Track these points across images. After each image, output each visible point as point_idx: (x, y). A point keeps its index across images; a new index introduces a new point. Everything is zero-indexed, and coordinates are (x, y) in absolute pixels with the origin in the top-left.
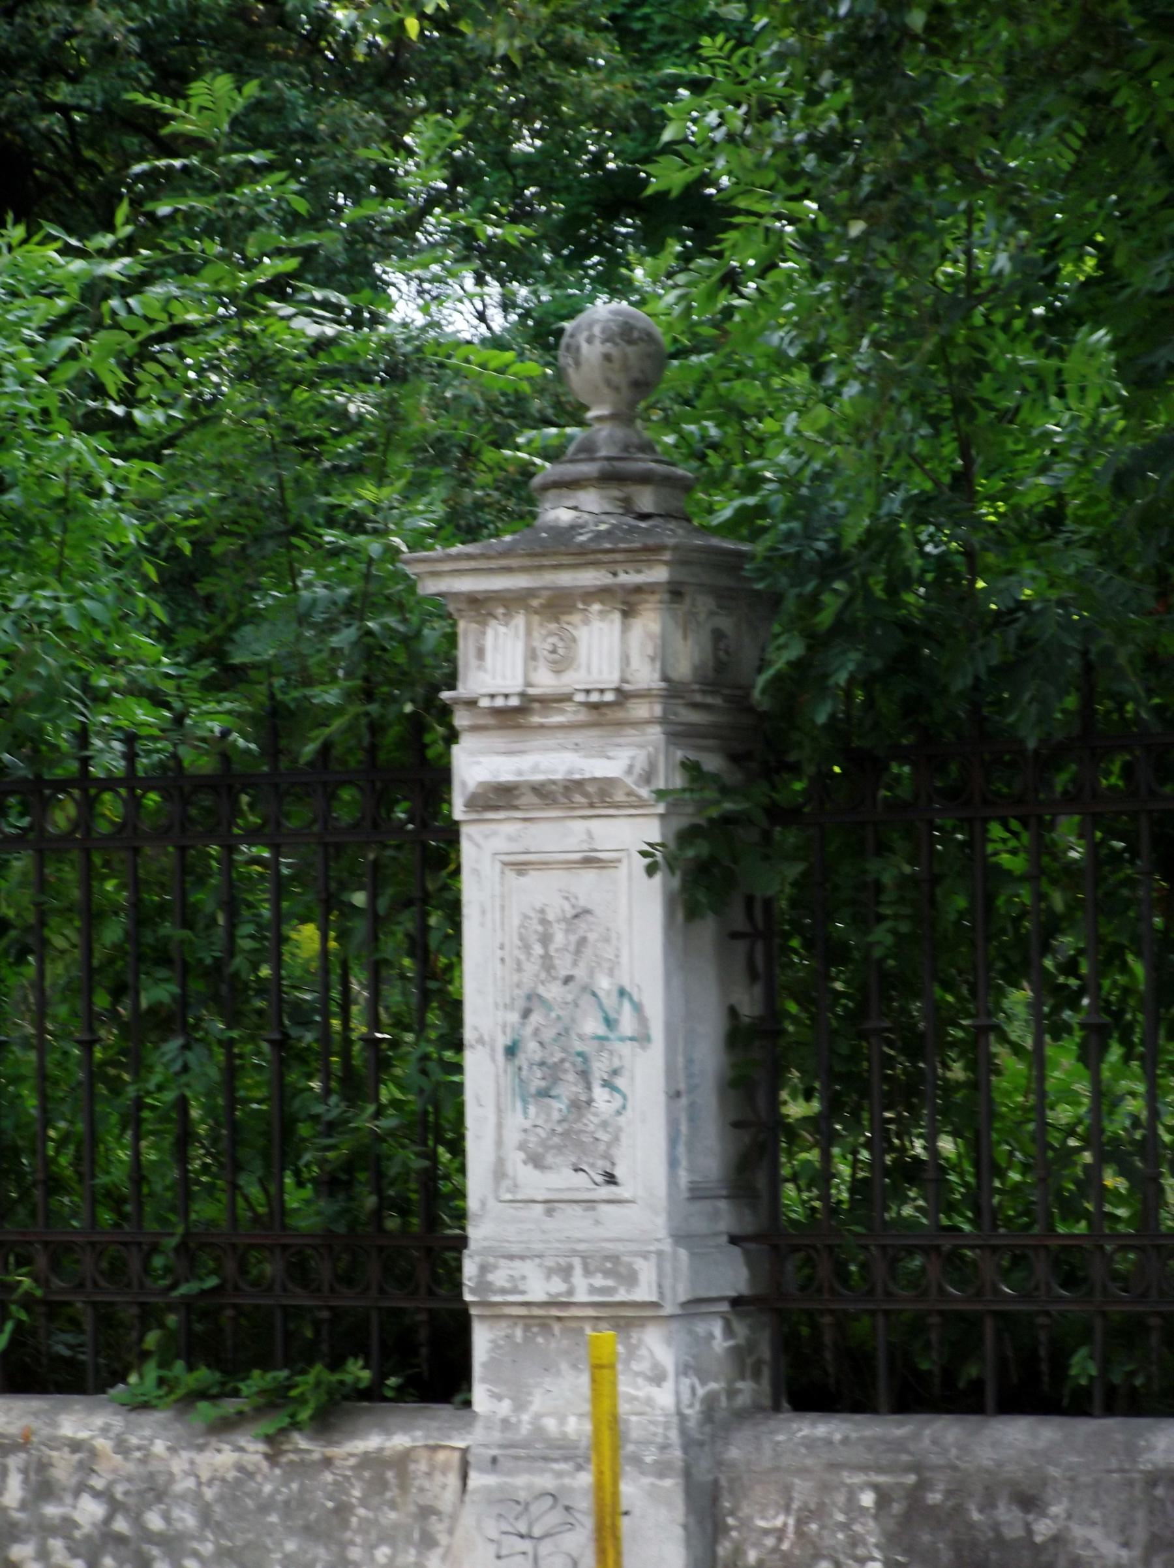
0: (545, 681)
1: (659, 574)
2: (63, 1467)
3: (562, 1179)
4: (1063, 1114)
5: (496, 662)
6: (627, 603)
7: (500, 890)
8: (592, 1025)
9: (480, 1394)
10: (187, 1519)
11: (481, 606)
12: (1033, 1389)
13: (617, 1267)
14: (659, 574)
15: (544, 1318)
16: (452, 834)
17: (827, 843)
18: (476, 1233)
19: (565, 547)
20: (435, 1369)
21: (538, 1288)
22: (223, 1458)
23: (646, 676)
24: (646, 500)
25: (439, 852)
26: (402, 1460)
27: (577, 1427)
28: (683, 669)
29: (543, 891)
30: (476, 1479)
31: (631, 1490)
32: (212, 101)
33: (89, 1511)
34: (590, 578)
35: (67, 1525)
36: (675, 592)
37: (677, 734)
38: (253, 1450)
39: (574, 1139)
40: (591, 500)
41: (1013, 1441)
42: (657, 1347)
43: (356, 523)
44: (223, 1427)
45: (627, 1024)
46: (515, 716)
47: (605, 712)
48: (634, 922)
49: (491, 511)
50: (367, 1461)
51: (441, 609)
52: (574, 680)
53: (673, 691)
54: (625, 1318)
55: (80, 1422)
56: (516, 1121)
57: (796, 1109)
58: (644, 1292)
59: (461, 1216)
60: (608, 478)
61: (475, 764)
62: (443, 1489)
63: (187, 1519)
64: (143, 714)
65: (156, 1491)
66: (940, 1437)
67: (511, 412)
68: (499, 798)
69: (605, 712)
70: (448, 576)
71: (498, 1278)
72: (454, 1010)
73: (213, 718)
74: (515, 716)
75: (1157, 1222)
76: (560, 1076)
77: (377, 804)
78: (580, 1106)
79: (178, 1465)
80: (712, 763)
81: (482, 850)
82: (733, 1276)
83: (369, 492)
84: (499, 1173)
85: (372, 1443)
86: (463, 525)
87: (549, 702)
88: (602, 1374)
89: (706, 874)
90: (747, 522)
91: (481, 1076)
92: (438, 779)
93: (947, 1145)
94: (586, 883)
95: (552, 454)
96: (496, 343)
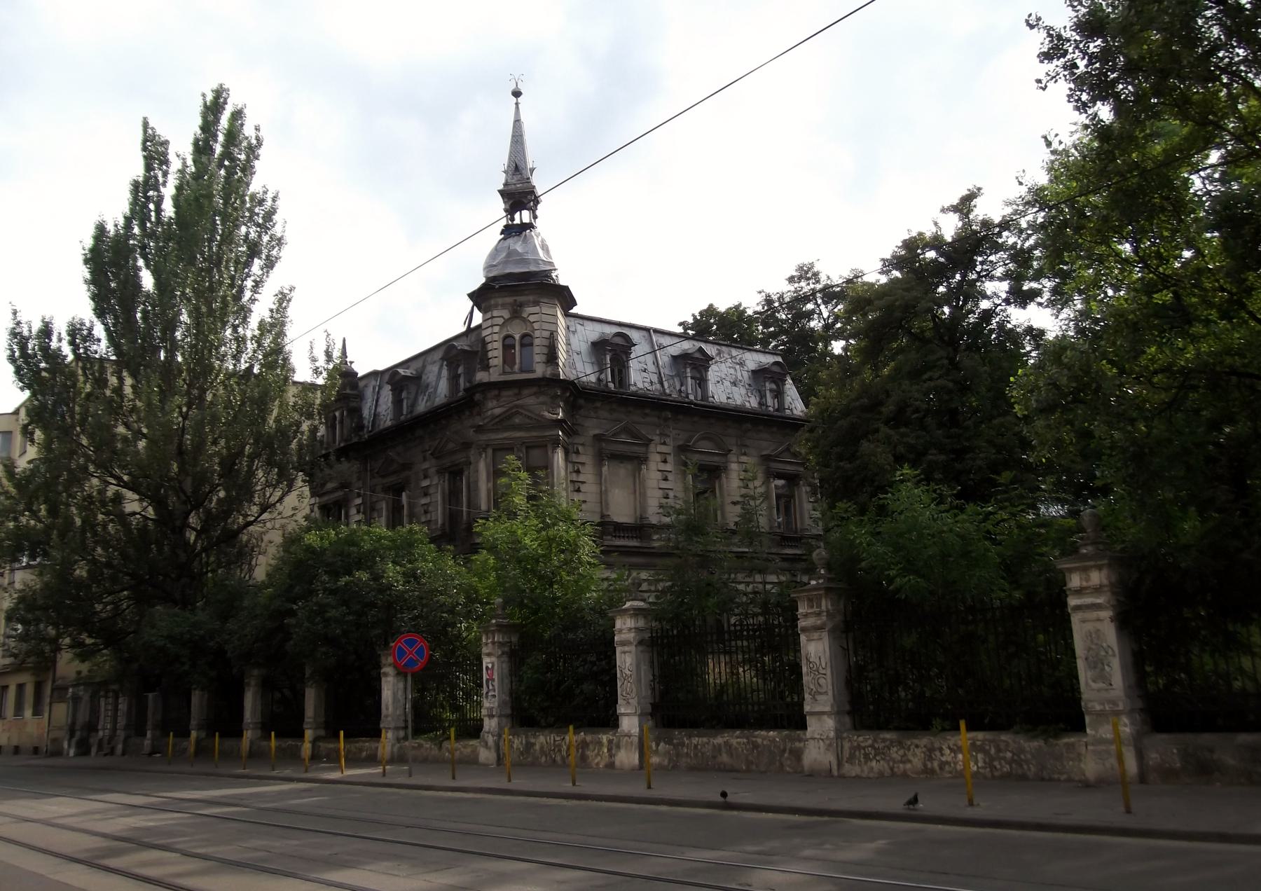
0: (1085, 584)
1: (1106, 562)
2: (1002, 746)
3: (1101, 685)
4: (1207, 668)
5: (1075, 581)
6: (1100, 568)
7: (1080, 628)
8: (1103, 653)
9: (1088, 731)
10: (1029, 756)
11: (1071, 570)
12: (1209, 725)
13: (1114, 703)
14: (1106, 562)
15: (1101, 715)
16: (1069, 615)
17: (1146, 613)
18: (1084, 696)
19: (1086, 558)
20: (1078, 726)
21: (1098, 708)
22: (1035, 744)
23: (1105, 582)
24: (1101, 547)
25: (1068, 621)
26: (1073, 745)
27: (1109, 736)
28: (1113, 579)
29: (1089, 626)
30: (1090, 748)
31: (1124, 749)
32: (1006, 476)
33: (1009, 755)
34: (1092, 563)
35: (1004, 758)
36: (1109, 565)
37: (1113, 593)
38: (1041, 743)
39: (1103, 677)
40: (1090, 548)
41: (1207, 738)
42: (1125, 720)
43: (1042, 555)
44: (1035, 737)
45: (1110, 652)
46: (1080, 592)
47: (1098, 590)
48: (1110, 634)
49: (1071, 551)
50: (1066, 744)
51: (1062, 571)
52: (1091, 584)
53: (1111, 584)
54: (1117, 714)
55: (1005, 737)
56: (1089, 674)
57: (1148, 669)
58: (1121, 708)
59: (1080, 693)
60: (1092, 544)
61: (1073, 601)
62: (1083, 750)
63: (1029, 756)
64: (1003, 594)
65: (1022, 751)
66: (1189, 737)
67: (1071, 532)
68: (1078, 608)
69: (1098, 590)
70: (1063, 565)
71: (1090, 705)
72: (1073, 651)
73: (1017, 594)
74: (1080, 592)
75: (896, 361)
76: (1097, 663)
77: (1053, 610)
78: (1103, 669)
79: (1026, 745)
80: (1122, 599)
81: (1075, 619)
82: (1139, 704)
83: (1045, 549)
84: (1087, 683)
85: (1066, 740)
86: (1064, 554)
87: (1086, 588)
88: (1115, 726)
89: (1124, 621)
90: (1123, 550)
91: (1081, 664)
92: (1065, 604)
93: (1183, 675)
94: (1098, 625)
95: (1081, 538)
96: (1062, 516)
